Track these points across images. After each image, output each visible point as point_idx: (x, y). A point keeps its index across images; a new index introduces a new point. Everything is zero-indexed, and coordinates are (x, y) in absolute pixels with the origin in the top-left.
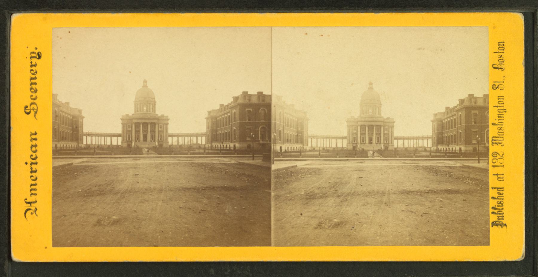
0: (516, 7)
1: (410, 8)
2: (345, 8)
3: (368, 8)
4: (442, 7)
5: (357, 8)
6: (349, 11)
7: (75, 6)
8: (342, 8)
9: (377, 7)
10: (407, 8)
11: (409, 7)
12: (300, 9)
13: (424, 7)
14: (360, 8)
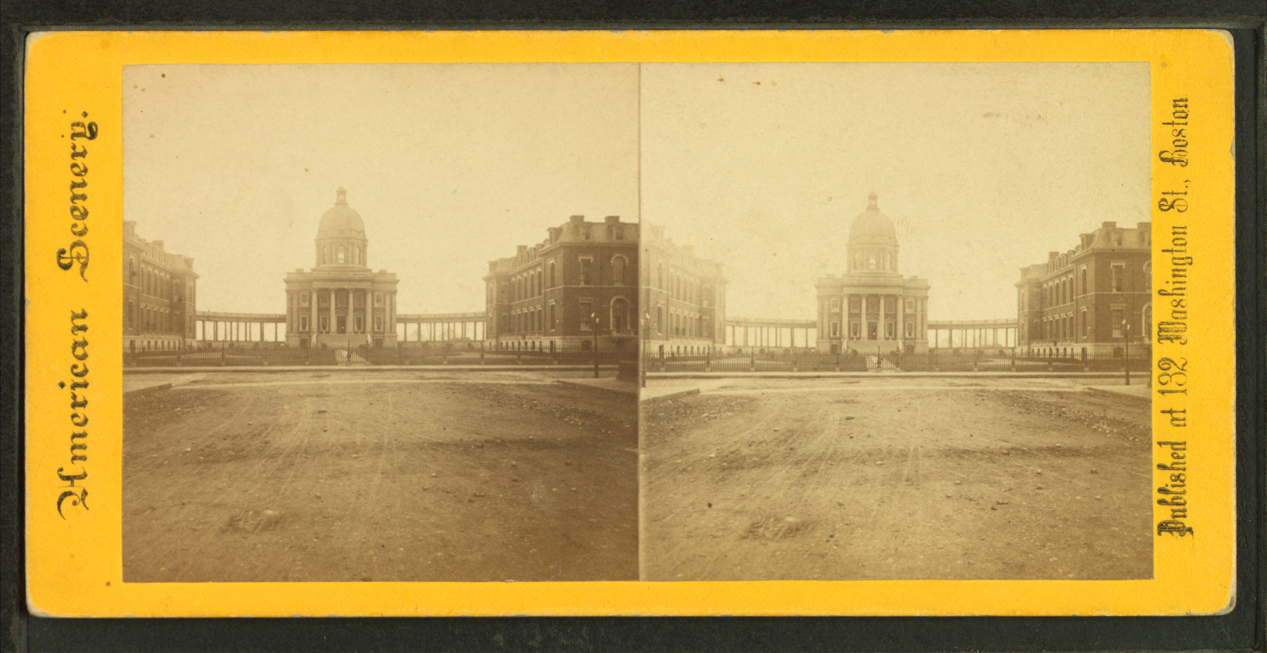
0: (1215, 16)
3: (867, 19)
4: (1041, 16)
5: (840, 19)
6: (823, 25)
7: (177, 13)
8: (806, 20)
9: (889, 17)
10: (958, 19)
11: (963, 17)
12: (705, 20)
14: (848, 18)
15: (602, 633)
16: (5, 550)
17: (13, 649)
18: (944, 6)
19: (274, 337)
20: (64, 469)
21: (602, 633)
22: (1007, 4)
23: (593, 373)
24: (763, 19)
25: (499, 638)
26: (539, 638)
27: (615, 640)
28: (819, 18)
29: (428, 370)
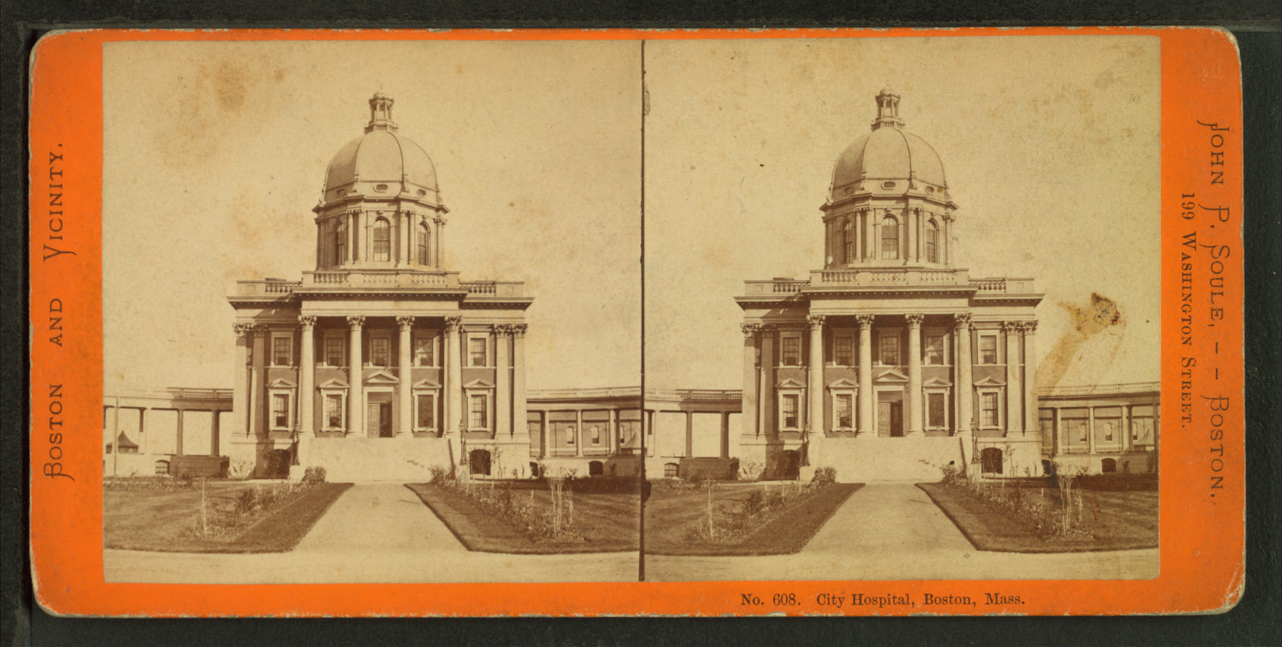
0: (1247, 19)
1: (993, 21)
2: (835, 20)
4: (1070, 18)
7: (187, 11)
8: (829, 21)
12: (727, 22)
13: (1026, 20)
14: (872, 20)
18: (970, 8)
24: (786, 21)
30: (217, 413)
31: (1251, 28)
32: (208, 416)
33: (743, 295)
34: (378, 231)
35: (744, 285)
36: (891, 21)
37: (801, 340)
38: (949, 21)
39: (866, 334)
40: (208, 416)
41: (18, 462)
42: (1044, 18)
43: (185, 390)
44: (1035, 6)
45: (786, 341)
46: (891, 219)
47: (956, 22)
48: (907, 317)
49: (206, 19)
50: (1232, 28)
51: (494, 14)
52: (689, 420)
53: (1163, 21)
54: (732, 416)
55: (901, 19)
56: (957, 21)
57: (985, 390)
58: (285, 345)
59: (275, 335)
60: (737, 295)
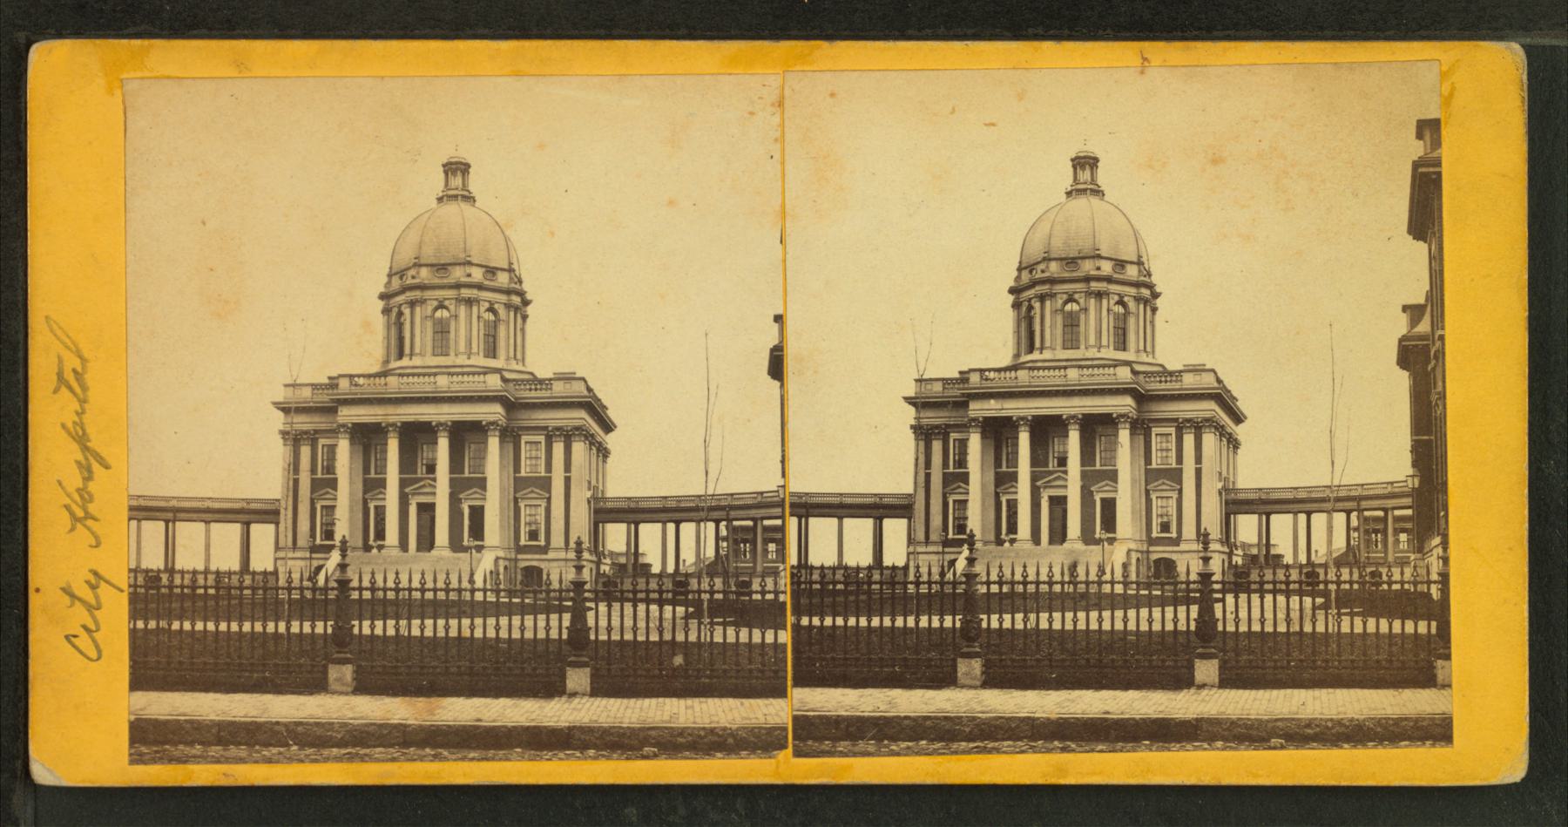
4: (1321, 28)
11: (1223, 30)
12: (897, 33)
15: (762, 806)
16: (6, 698)
17: (16, 823)
18: (1199, 16)
19: (143, 534)
20: (40, 594)
21: (762, 806)
22: (1278, 13)
23: (132, 582)
25: (632, 812)
26: (682, 811)
27: (778, 816)
28: (1040, 31)
29: (1042, 331)
30: (247, 524)
31: (1547, 41)
32: (237, 528)
33: (281, 400)
34: (487, 323)
35: (283, 388)
36: (1100, 32)
37: (1174, 436)
38: (1171, 32)
39: (1024, 438)
40: (237, 528)
41: (19, 578)
42: (1290, 29)
43: (1395, 485)
44: (1278, 13)
45: (1159, 438)
46: (444, 311)
47: (1180, 34)
48: (434, 424)
49: (252, 29)
50: (1523, 40)
51: (609, 23)
52: (426, 533)
53: (815, 31)
54: (642, 527)
55: (1114, 30)
56: (1183, 32)
57: (1159, 494)
58: (537, 450)
59: (953, 436)
60: (907, 395)
